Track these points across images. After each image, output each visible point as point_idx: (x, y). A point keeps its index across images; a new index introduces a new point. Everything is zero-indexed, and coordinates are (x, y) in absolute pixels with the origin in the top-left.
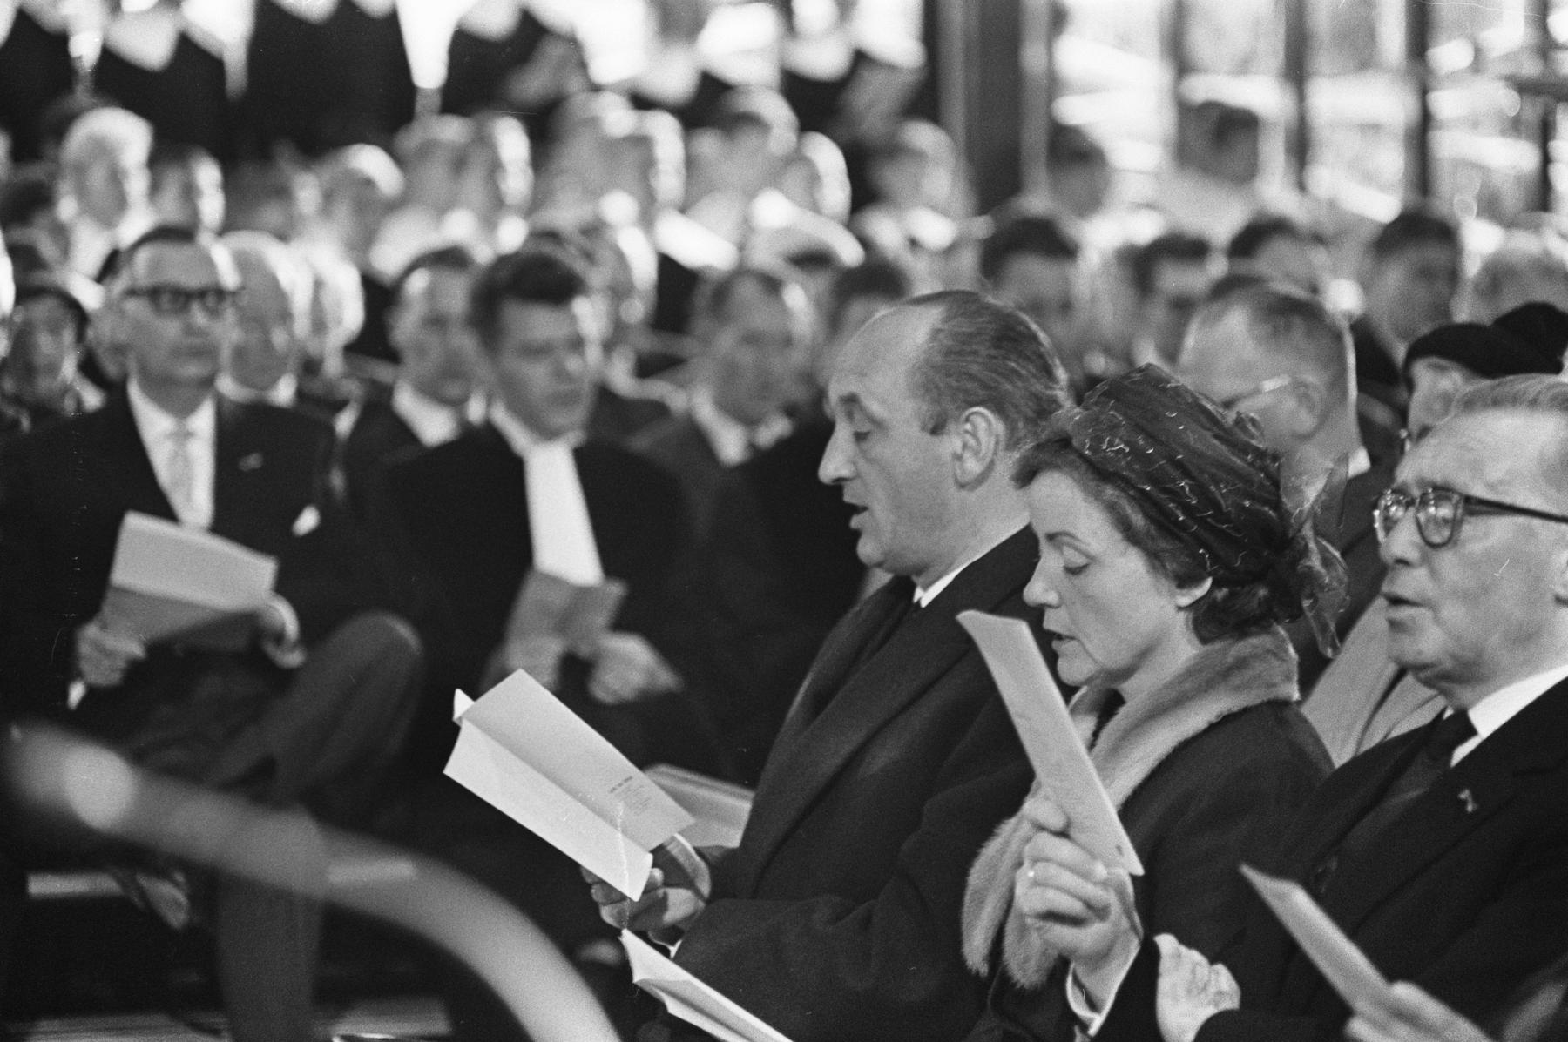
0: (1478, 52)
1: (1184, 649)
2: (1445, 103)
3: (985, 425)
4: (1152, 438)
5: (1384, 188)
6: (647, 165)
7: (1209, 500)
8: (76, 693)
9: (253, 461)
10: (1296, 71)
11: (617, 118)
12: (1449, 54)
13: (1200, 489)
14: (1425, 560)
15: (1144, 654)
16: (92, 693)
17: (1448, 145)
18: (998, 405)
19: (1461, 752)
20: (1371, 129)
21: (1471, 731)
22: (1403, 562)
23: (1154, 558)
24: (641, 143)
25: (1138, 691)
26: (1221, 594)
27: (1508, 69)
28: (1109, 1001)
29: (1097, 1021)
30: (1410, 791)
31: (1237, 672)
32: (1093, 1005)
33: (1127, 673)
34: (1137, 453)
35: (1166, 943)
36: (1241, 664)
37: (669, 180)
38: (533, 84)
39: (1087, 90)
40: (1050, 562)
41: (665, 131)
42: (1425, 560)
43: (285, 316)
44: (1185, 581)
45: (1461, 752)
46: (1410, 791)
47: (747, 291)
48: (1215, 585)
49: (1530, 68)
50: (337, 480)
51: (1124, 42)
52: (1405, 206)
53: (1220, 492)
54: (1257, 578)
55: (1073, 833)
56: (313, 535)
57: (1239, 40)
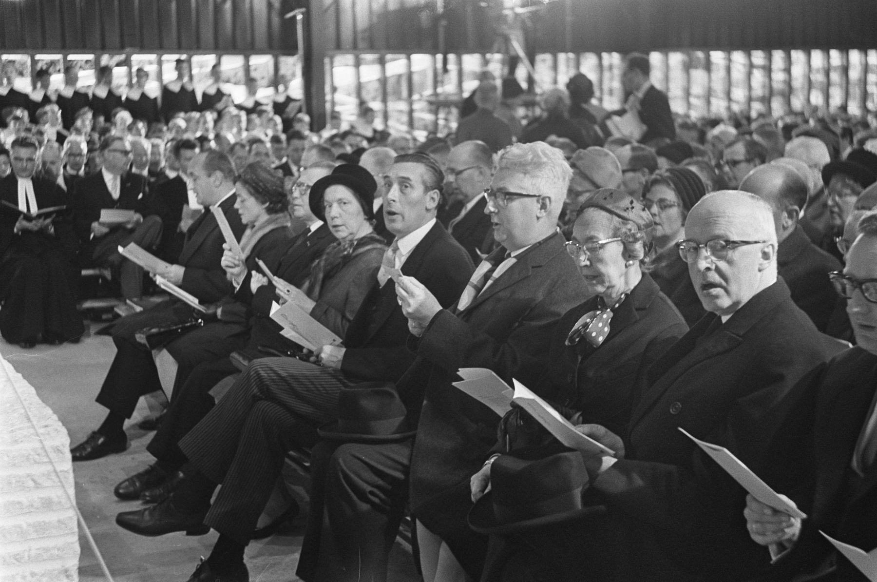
0: (421, 96)
1: (265, 217)
2: (416, 106)
3: (219, 174)
4: (256, 175)
5: (402, 123)
6: (240, 122)
7: (266, 187)
8: (92, 236)
9: (129, 185)
10: (384, 101)
11: (234, 111)
12: (416, 97)
13: (265, 185)
14: (301, 197)
15: (258, 217)
16: (94, 237)
17: (416, 115)
18: (221, 170)
19: (309, 234)
20: (401, 111)
21: (310, 231)
22: (296, 198)
23: (257, 198)
24: (238, 116)
25: (257, 224)
26: (272, 205)
27: (427, 99)
28: (241, 284)
29: (238, 287)
30: (299, 242)
31: (515, 240)
32: (238, 284)
33: (255, 221)
34: (252, 178)
35: (254, 273)
36: (277, 219)
37: (244, 125)
38: (220, 106)
39: (342, 104)
40: (239, 200)
41: (243, 114)
42: (301, 197)
43: (146, 154)
44: (263, 203)
45: (309, 234)
46: (299, 242)
47: (237, 148)
48: (270, 204)
49: (433, 99)
50: (147, 189)
51: (349, 95)
52: (731, 125)
53: (268, 185)
54: (280, 202)
55: (232, 250)
56: (142, 199)
57: (372, 94)
